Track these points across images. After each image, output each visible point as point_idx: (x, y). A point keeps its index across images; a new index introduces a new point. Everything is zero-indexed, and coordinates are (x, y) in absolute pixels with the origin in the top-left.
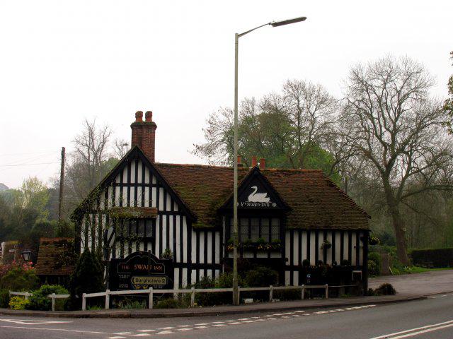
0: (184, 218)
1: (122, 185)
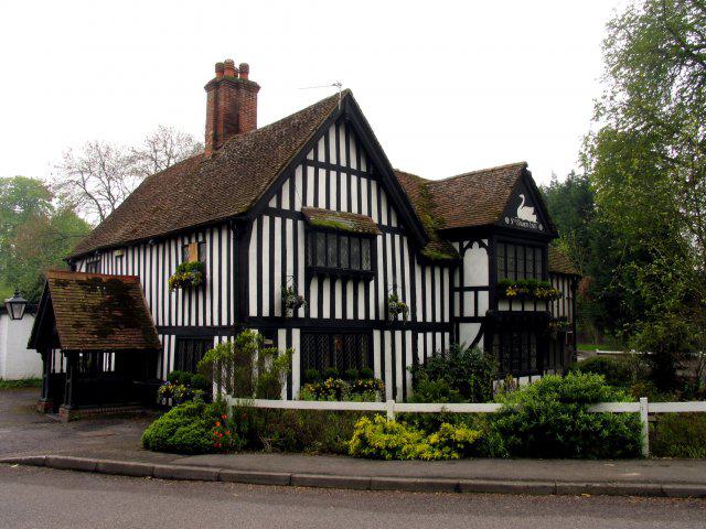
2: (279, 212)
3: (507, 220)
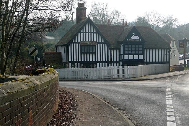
0: (106, 45)
1: (83, 33)
2: (75, 42)
3: (127, 40)
